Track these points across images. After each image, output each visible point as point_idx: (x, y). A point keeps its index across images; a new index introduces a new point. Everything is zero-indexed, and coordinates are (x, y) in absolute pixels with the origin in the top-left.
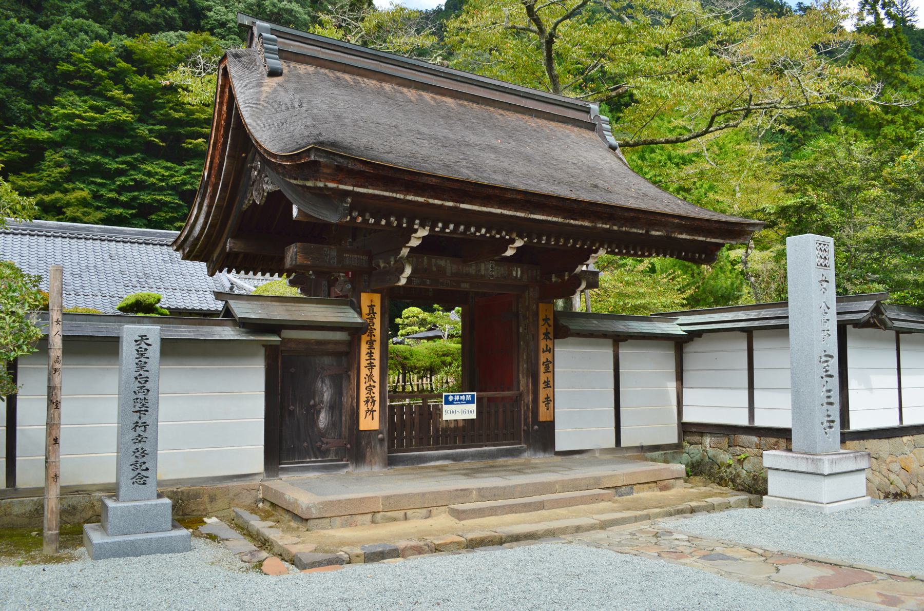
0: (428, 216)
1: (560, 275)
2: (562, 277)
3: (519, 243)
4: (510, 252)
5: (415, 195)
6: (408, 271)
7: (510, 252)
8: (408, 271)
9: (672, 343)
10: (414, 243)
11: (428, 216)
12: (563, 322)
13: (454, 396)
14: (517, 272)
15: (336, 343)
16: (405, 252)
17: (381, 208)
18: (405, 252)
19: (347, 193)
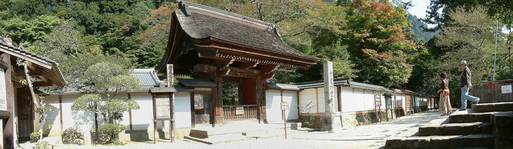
0: (237, 55)
1: (267, 72)
2: (223, 68)
3: (233, 60)
4: (255, 66)
5: (205, 47)
6: (229, 71)
7: (255, 66)
8: (229, 71)
9: (296, 92)
10: (231, 63)
11: (237, 55)
12: (268, 85)
13: (24, 61)
14: (255, 72)
15: (208, 91)
16: (228, 65)
17: (225, 53)
18: (228, 65)
19: (217, 49)
